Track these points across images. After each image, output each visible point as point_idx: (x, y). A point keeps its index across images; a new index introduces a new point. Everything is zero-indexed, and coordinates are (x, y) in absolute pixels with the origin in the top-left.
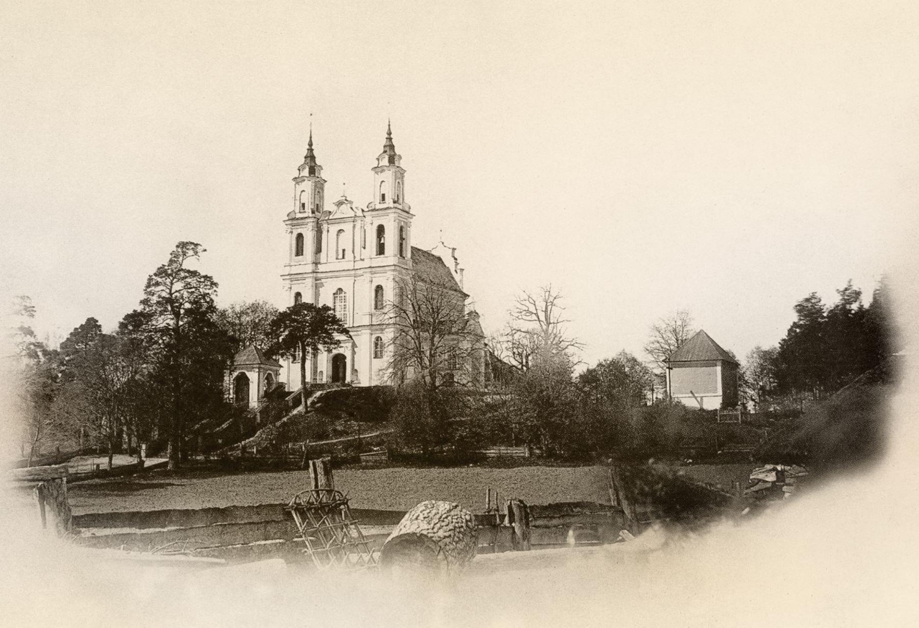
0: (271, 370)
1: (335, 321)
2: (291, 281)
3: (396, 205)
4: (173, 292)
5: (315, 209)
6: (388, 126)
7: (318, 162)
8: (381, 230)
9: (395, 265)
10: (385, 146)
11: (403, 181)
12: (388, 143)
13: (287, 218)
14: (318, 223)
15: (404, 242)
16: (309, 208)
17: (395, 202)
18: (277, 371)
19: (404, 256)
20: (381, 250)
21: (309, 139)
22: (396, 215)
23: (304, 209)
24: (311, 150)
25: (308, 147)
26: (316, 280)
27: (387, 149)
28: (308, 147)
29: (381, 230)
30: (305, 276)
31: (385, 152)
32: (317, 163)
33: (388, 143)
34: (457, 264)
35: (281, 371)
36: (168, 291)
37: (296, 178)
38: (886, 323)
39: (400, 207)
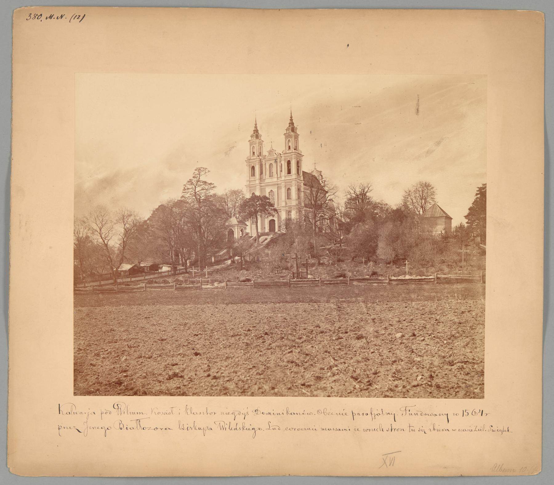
0: (243, 227)
1: (272, 205)
6: (255, 122)
7: (295, 125)
10: (289, 124)
11: (298, 140)
12: (255, 129)
13: (247, 159)
14: (260, 161)
17: (295, 149)
20: (289, 172)
21: (290, 114)
22: (295, 155)
23: (254, 155)
25: (290, 119)
26: (261, 187)
27: (291, 125)
31: (290, 126)
32: (295, 126)
33: (291, 122)
36: (194, 191)
37: (250, 140)
39: (297, 152)
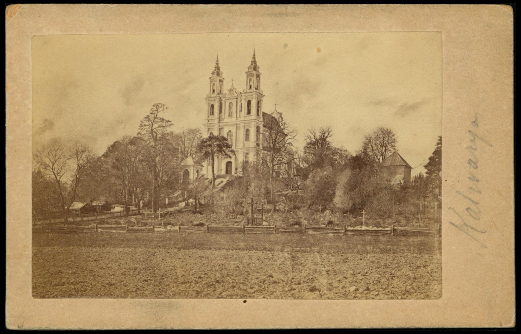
2: (244, 123)
3: (256, 91)
4: (153, 128)
5: (219, 93)
8: (249, 103)
9: (255, 119)
15: (259, 109)
16: (217, 92)
18: (201, 168)
19: (259, 115)
20: (249, 112)
21: (216, 58)
22: (256, 95)
24: (254, 58)
27: (253, 63)
28: (253, 57)
29: (249, 103)
30: (251, 121)
33: (253, 60)
34: (282, 120)
35: (203, 169)
38: (441, 167)
